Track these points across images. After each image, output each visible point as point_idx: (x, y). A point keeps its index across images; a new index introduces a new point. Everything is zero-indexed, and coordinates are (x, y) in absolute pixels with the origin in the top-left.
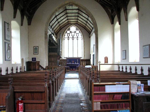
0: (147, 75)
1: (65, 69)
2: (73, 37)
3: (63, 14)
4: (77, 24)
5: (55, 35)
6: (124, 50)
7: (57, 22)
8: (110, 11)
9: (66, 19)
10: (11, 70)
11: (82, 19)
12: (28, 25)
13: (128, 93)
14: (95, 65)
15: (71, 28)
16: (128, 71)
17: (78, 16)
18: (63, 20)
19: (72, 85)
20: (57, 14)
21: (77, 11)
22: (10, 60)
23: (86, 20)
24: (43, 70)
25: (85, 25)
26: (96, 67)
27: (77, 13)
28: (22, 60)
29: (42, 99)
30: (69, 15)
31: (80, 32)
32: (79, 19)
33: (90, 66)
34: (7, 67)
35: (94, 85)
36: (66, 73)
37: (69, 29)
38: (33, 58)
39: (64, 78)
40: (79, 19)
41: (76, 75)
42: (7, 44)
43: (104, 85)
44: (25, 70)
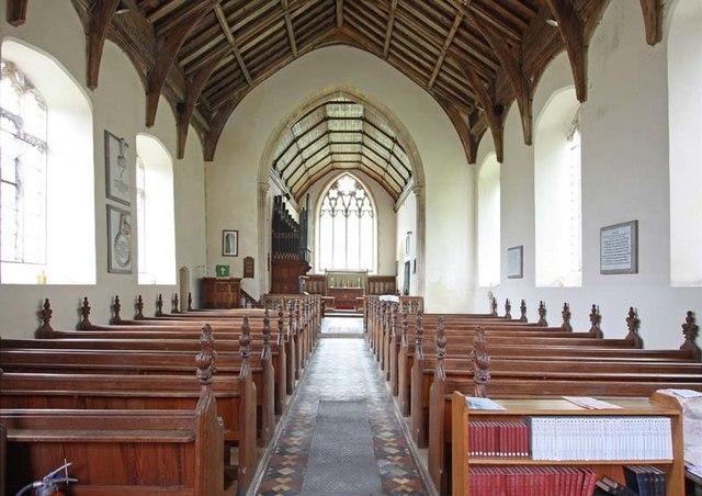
0: (560, 326)
1: (323, 305)
2: (346, 210)
3: (317, 133)
4: (358, 170)
5: (292, 199)
6: (628, 224)
7: (298, 161)
8: (466, 119)
9: (322, 142)
10: (79, 310)
11: (373, 159)
12: (206, 160)
13: (667, 468)
14: (412, 293)
15: (340, 182)
16: (533, 318)
17: (362, 144)
18: (319, 159)
19: (343, 364)
20: (298, 132)
21: (358, 126)
22: (130, 269)
23: (385, 154)
24: (253, 307)
25: (382, 173)
26: (418, 301)
27: (360, 131)
28: (182, 273)
29: (180, 480)
30: (335, 137)
31: (366, 194)
32: (367, 152)
33: (395, 299)
34: (47, 300)
35: (470, 415)
36: (324, 316)
37: (335, 186)
38: (218, 268)
39: (316, 335)
40: (367, 152)
41: (355, 324)
42: (115, 216)
43: (527, 418)
44: (193, 306)
